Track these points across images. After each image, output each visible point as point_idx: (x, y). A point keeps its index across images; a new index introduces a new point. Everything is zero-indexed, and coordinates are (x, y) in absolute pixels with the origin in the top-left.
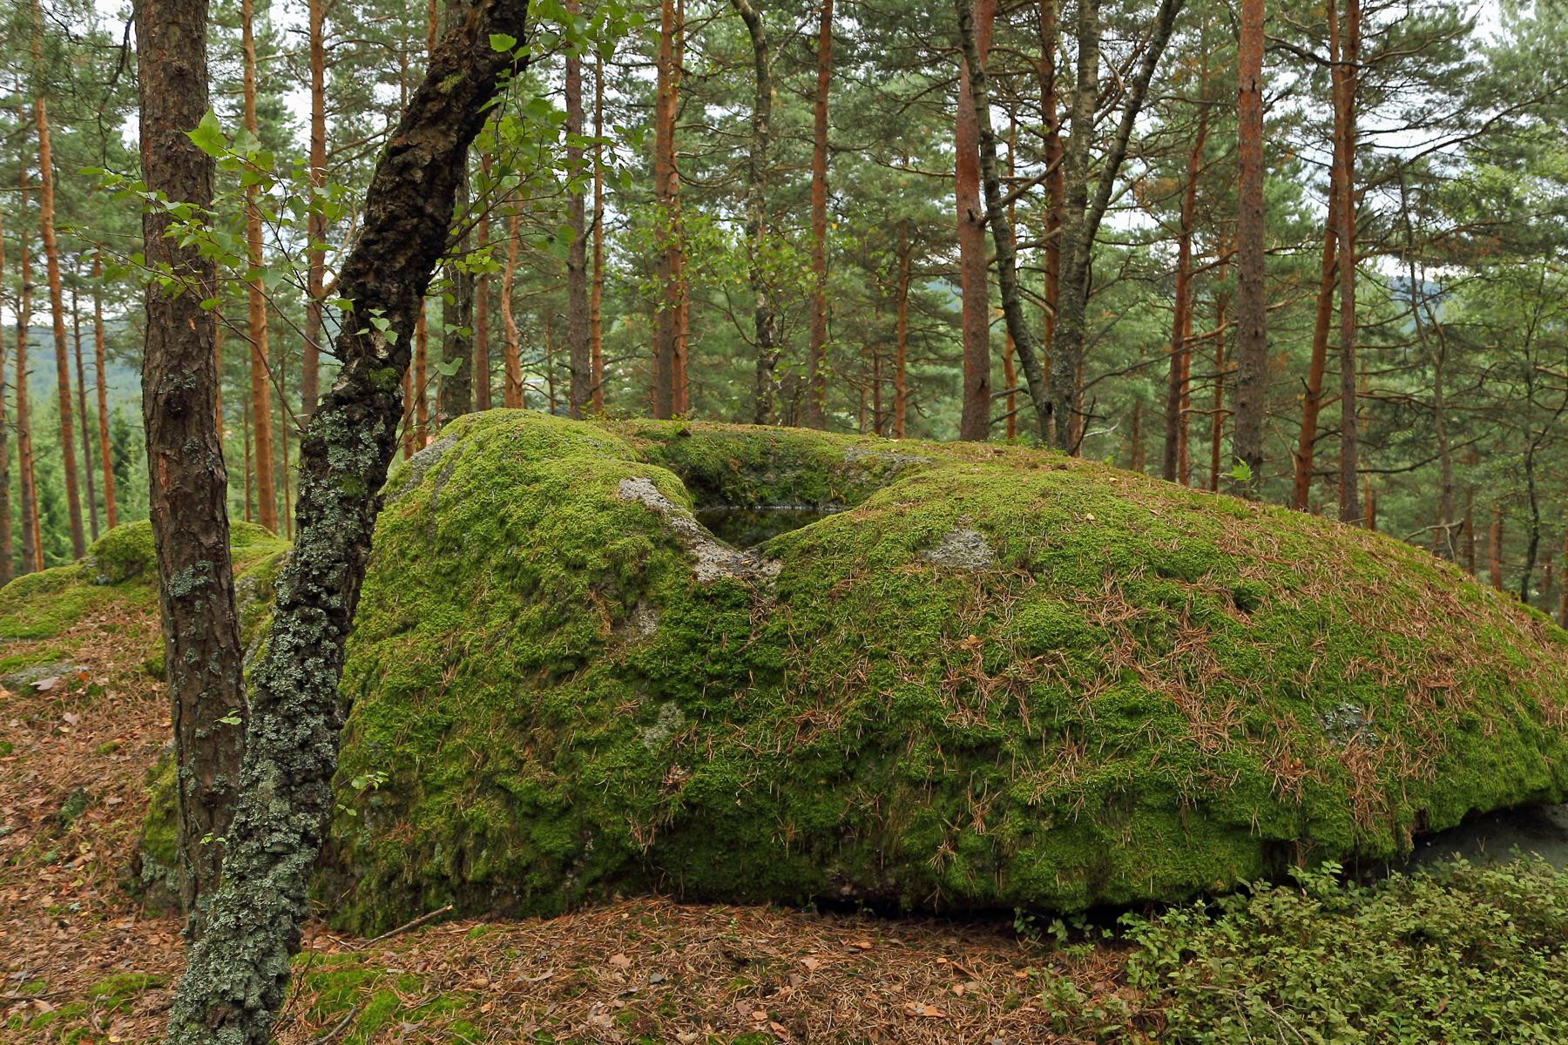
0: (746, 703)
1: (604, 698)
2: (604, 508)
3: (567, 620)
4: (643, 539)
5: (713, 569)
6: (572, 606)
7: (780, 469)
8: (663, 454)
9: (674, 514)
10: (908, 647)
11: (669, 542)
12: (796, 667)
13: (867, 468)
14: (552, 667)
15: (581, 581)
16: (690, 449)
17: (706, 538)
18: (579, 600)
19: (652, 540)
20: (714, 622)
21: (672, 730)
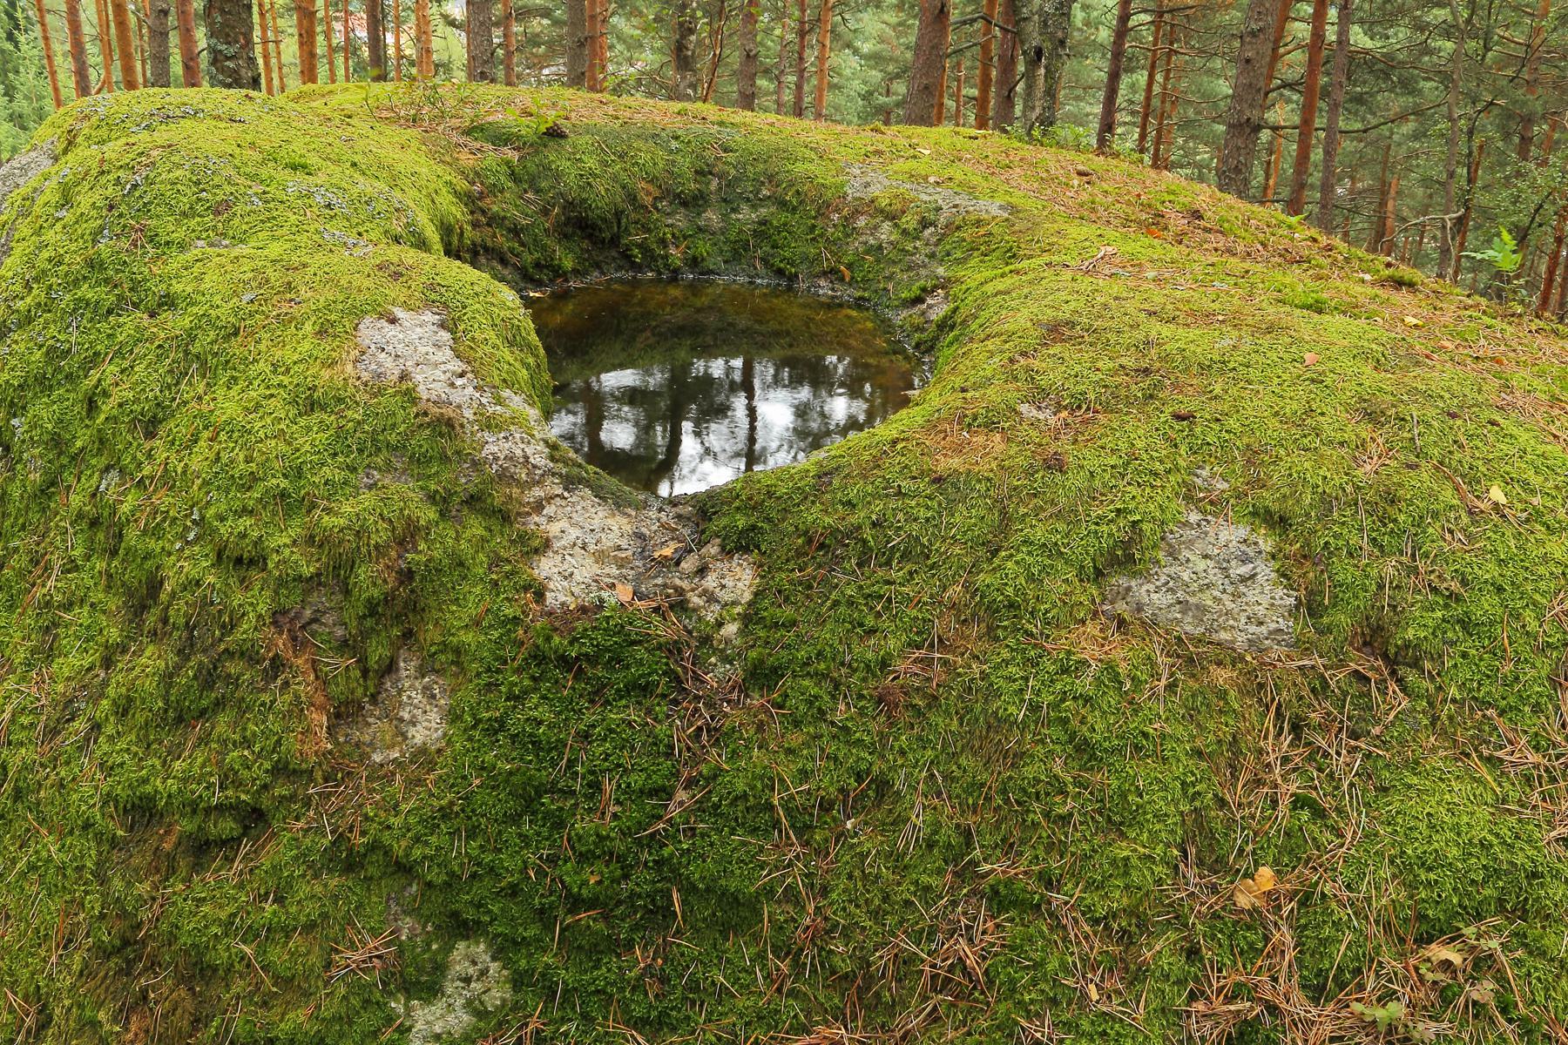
0: (664, 980)
1: (310, 927)
2: (312, 406)
3: (219, 704)
4: (408, 496)
5: (586, 570)
6: (232, 668)
7: (729, 203)
8: (513, 175)
9: (489, 424)
10: (1091, 885)
11: (474, 501)
12: (791, 895)
13: (892, 217)
14: (186, 825)
15: (254, 602)
16: (564, 164)
17: (570, 483)
18: (249, 655)
19: (431, 498)
20: (585, 736)
21: (481, 1014)
